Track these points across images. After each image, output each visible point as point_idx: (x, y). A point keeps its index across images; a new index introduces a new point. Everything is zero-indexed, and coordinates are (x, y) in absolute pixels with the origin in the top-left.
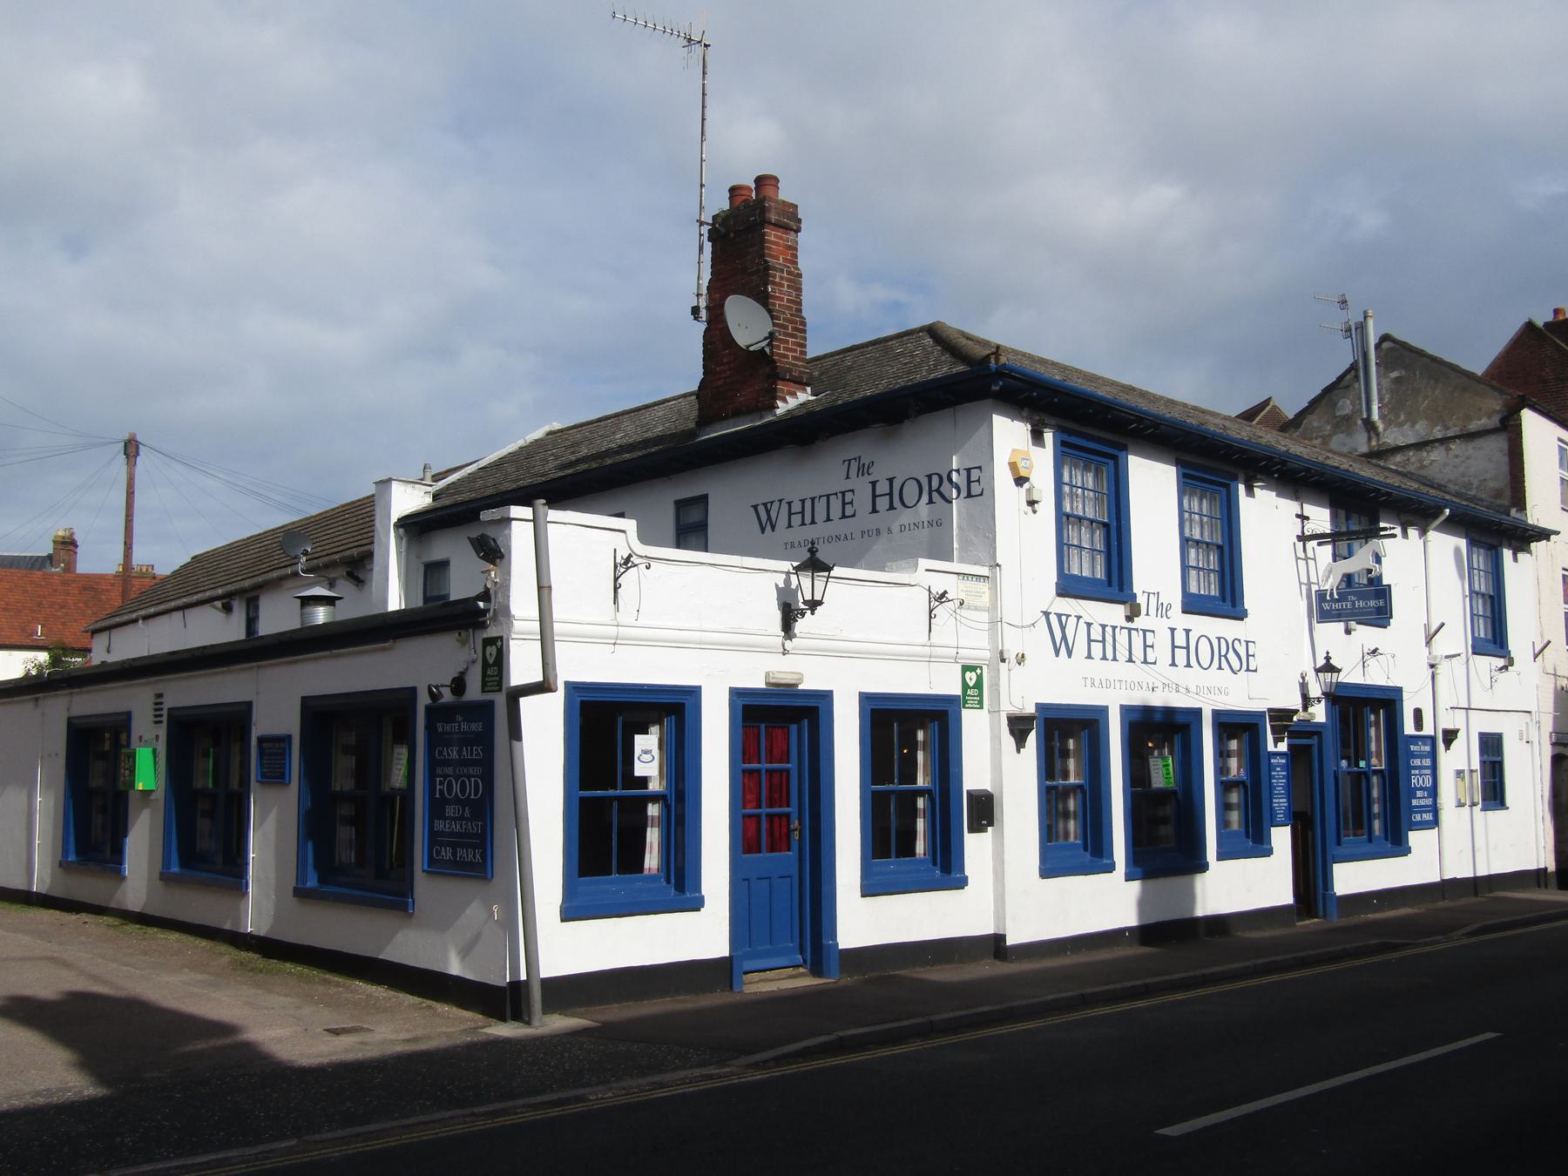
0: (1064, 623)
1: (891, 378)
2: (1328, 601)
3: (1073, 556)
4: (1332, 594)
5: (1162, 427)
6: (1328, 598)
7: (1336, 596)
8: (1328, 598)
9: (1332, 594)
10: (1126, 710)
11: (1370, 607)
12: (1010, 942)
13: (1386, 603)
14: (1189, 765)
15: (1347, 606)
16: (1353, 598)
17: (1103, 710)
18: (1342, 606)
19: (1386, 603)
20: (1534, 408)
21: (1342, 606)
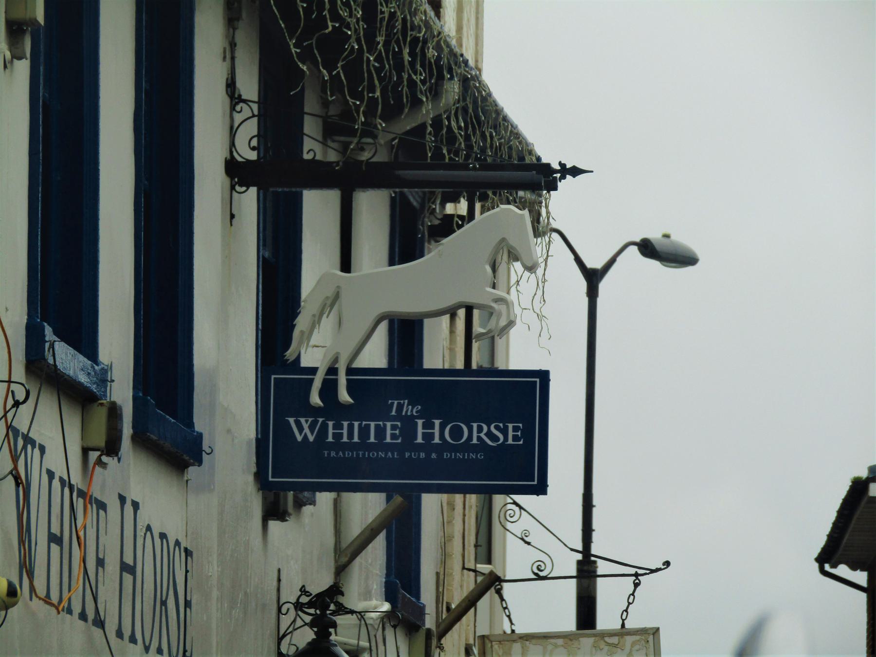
0: (6, 440)
1: (338, 505)
2: (315, 412)
3: (470, 511)
4: (329, 388)
5: (392, 624)
6: (315, 399)
7: (344, 396)
8: (315, 399)
9: (329, 388)
10: (333, 430)
11: (467, 446)
12: (568, 167)
13: (528, 433)
14: (361, 346)
15: (381, 432)
16: (408, 410)
17: (343, 430)
18: (364, 432)
19: (528, 433)
20: (131, 566)
21: (364, 432)
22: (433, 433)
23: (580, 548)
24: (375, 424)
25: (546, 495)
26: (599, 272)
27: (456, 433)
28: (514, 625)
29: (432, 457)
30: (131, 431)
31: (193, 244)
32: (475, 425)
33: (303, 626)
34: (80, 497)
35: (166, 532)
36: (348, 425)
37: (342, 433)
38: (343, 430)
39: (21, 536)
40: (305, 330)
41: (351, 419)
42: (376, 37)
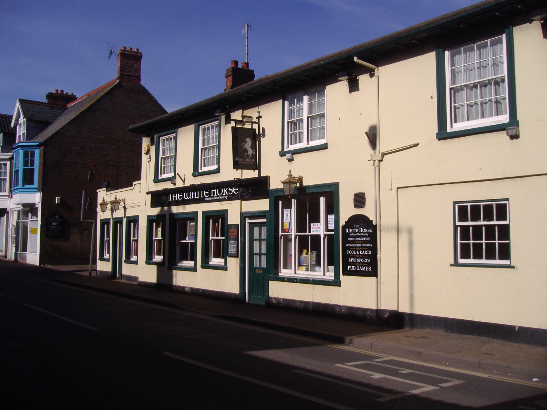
22: (482, 258)
23: (430, 58)
24: (239, 224)
25: (233, 169)
26: (103, 258)
27: (364, 230)
28: (236, 63)
29: (297, 193)
30: (495, 217)
31: (414, 57)
32: (176, 200)
33: (10, 201)
34: (186, 239)
35: (145, 263)
36: (176, 199)
37: (468, 221)
38: (324, 111)
39: (233, 255)
40: (257, 78)
41: (350, 233)
42: (15, 236)
